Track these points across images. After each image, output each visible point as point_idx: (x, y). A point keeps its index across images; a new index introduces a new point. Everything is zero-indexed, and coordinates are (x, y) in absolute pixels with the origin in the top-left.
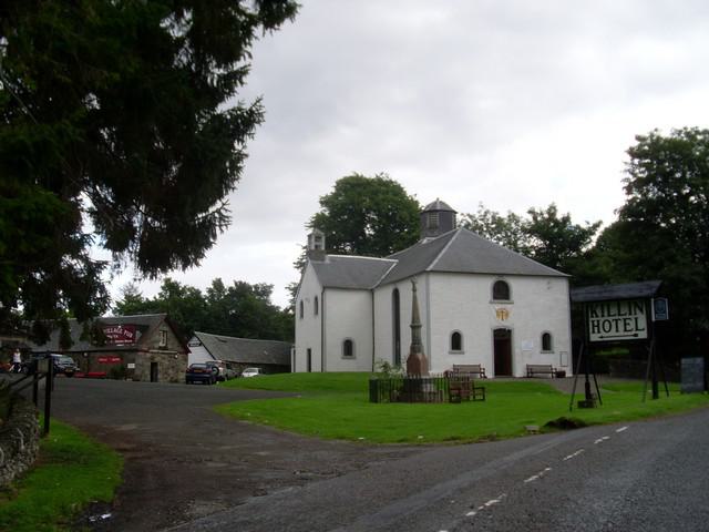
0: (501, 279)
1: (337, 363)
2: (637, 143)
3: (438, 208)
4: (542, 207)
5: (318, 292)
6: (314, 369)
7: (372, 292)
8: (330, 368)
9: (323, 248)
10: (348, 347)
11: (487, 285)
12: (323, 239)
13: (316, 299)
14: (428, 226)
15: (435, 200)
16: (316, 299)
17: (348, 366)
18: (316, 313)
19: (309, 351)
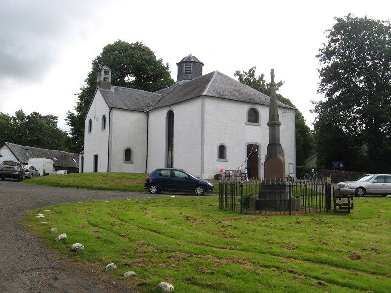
0: (253, 107)
1: (120, 167)
2: (377, 21)
3: (192, 60)
4: (245, 69)
5: (106, 111)
6: (99, 170)
7: (147, 114)
8: (115, 170)
9: (110, 80)
10: (128, 155)
11: (245, 109)
12: (110, 73)
13: (104, 117)
14: (184, 72)
15: (188, 55)
16: (104, 117)
17: (128, 168)
18: (104, 128)
19: (96, 157)
